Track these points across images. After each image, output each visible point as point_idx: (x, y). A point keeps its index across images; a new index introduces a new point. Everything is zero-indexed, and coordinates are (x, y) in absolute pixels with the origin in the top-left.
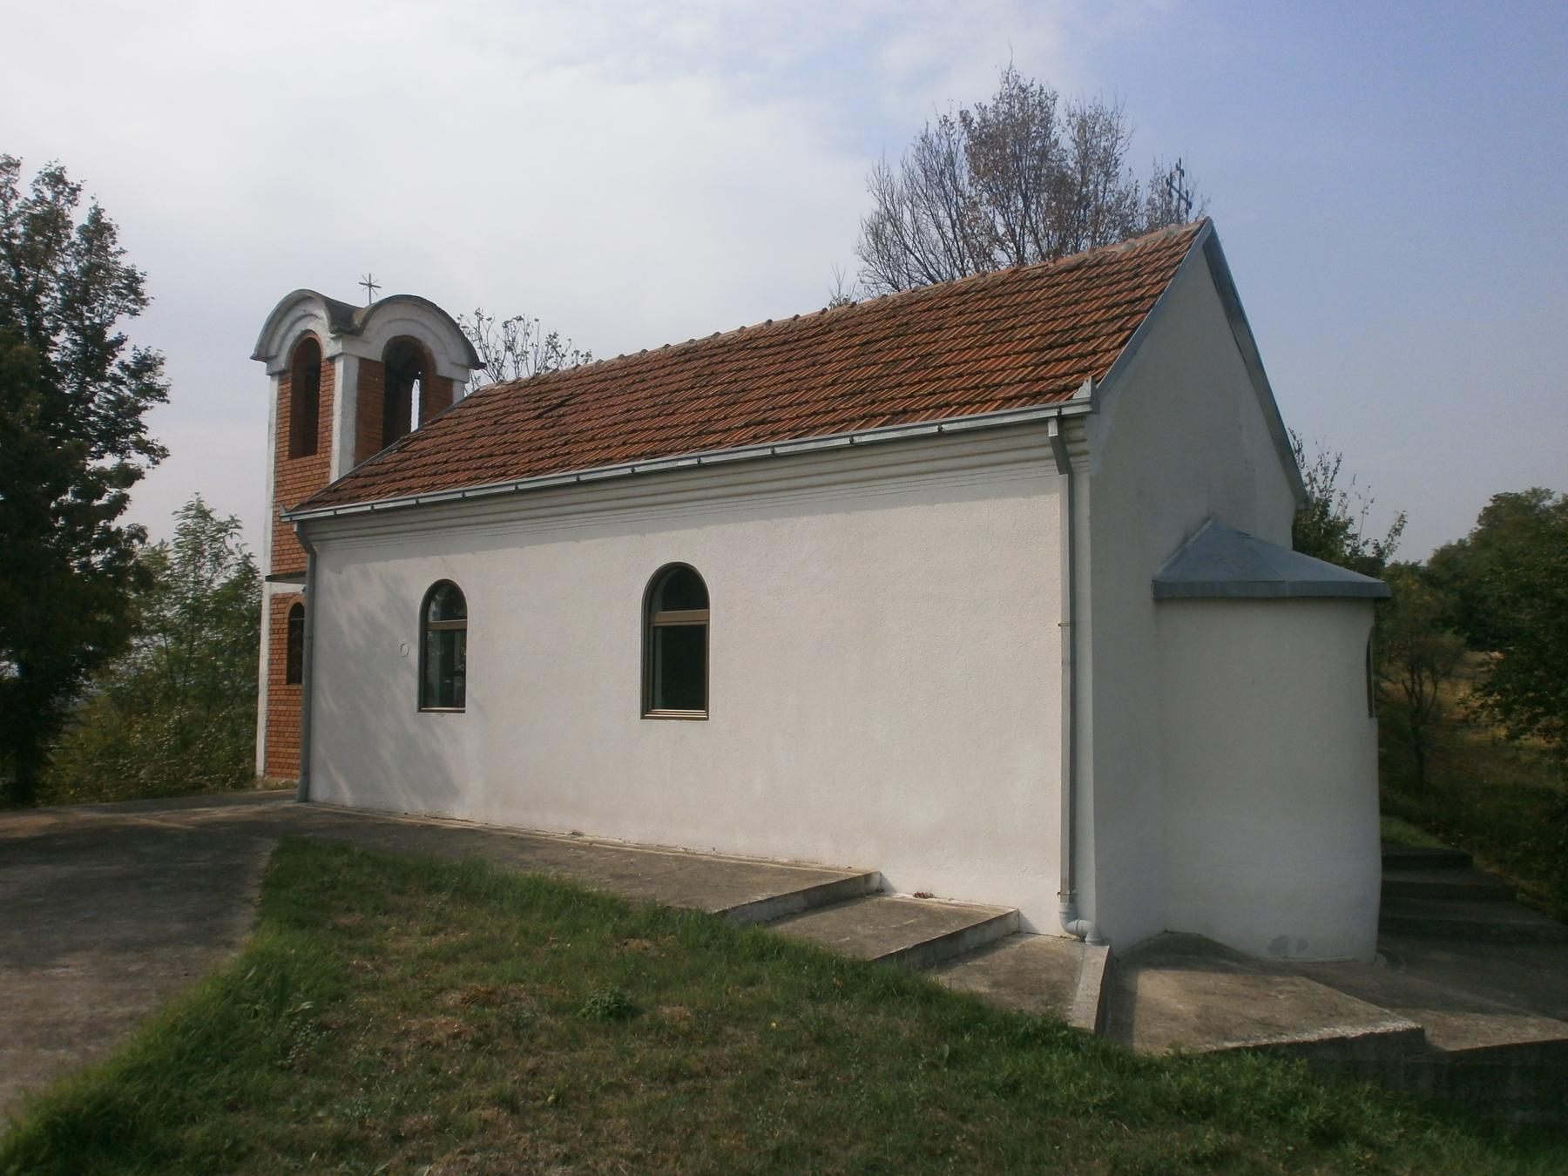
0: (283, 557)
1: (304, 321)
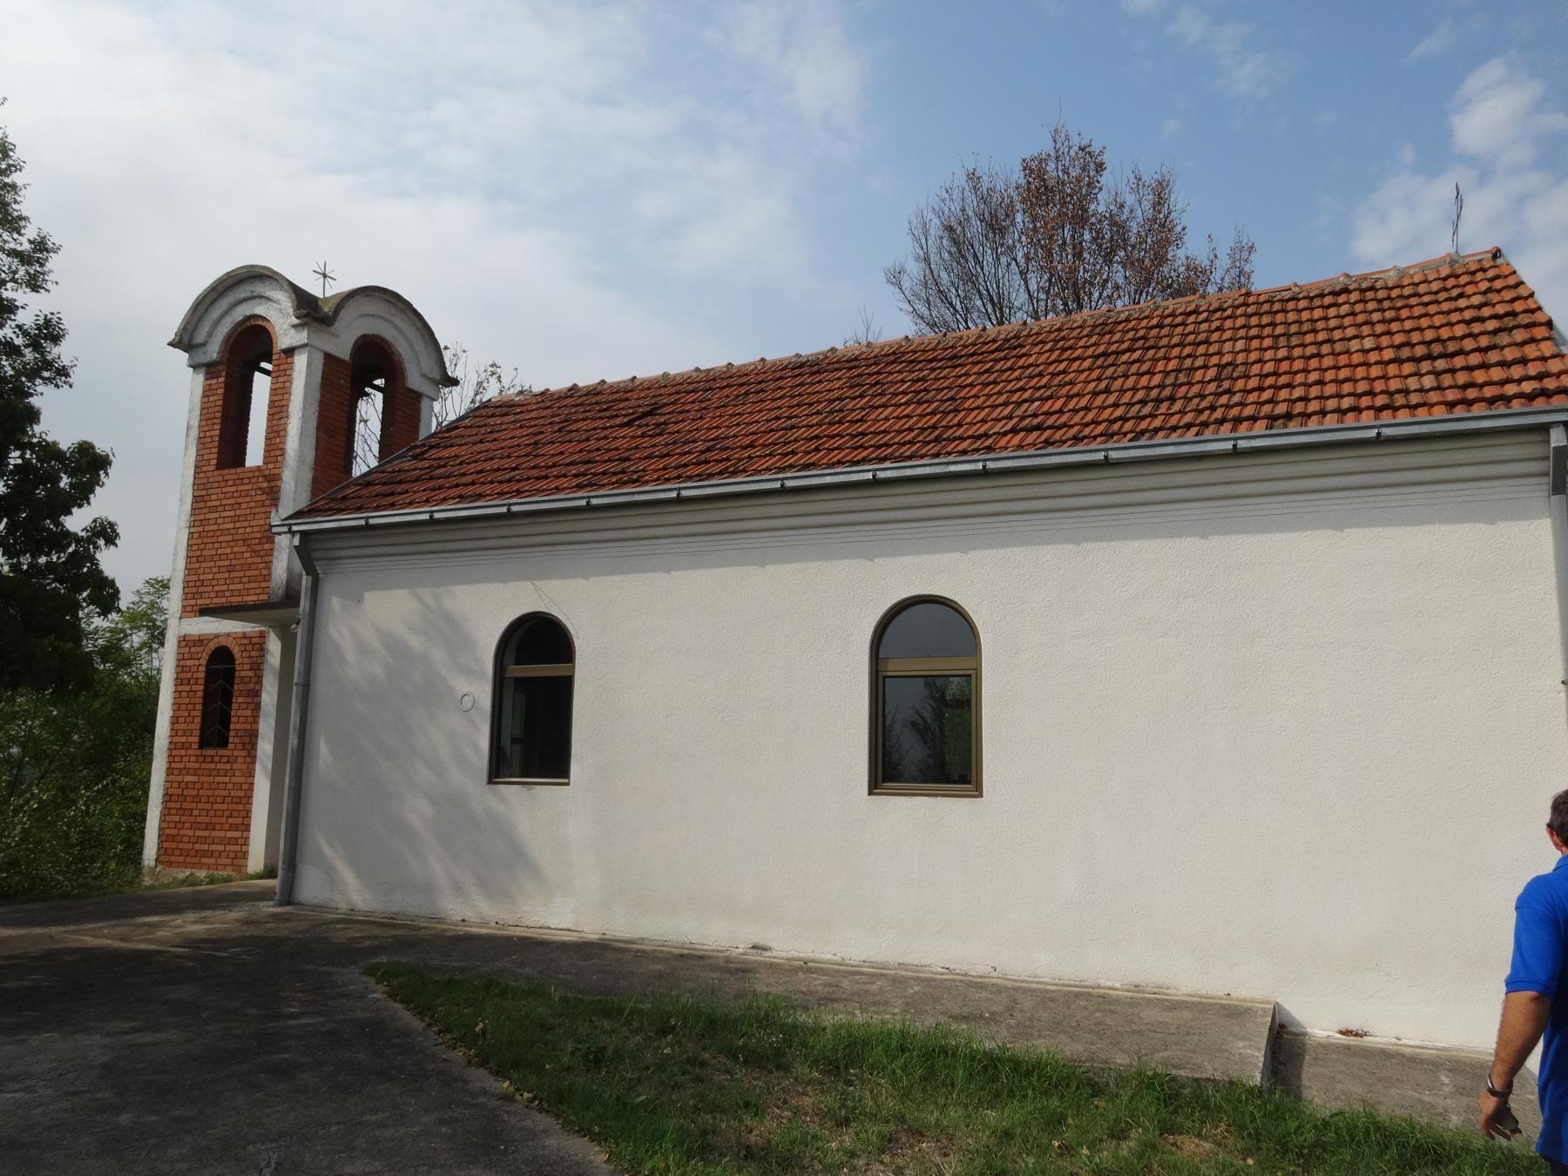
0: (201, 590)
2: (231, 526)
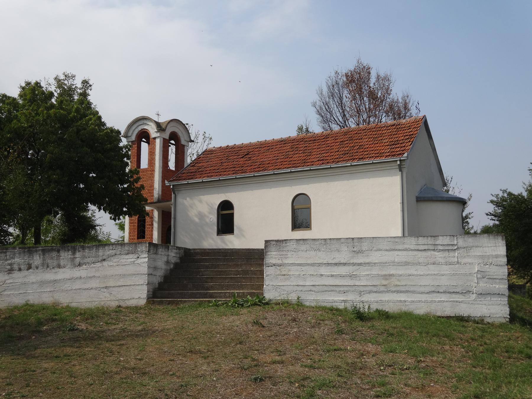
1: (143, 125)
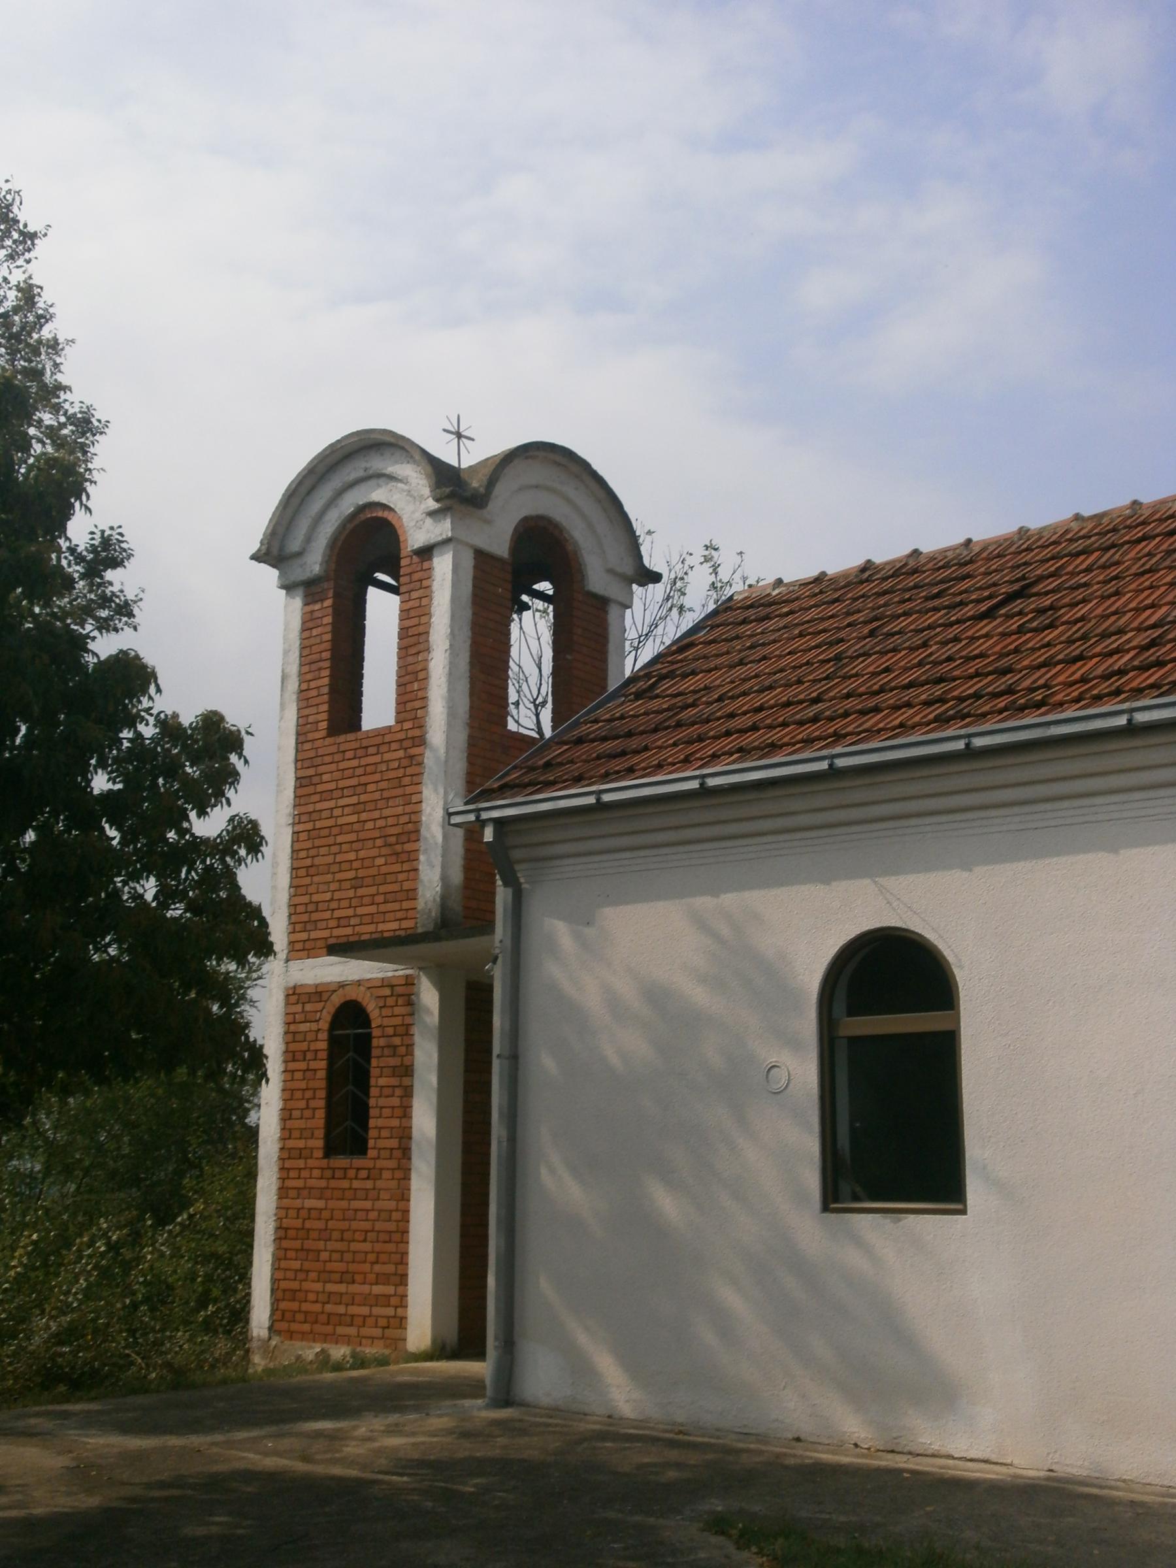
0: (315, 916)
2: (354, 818)
